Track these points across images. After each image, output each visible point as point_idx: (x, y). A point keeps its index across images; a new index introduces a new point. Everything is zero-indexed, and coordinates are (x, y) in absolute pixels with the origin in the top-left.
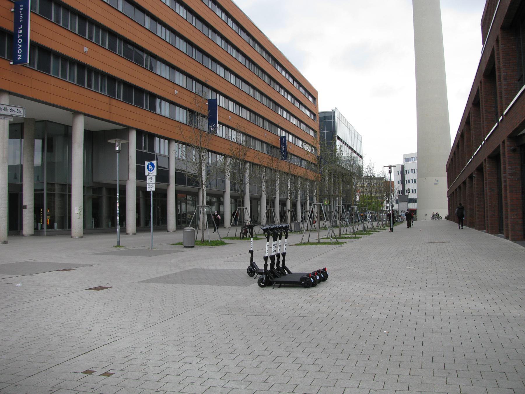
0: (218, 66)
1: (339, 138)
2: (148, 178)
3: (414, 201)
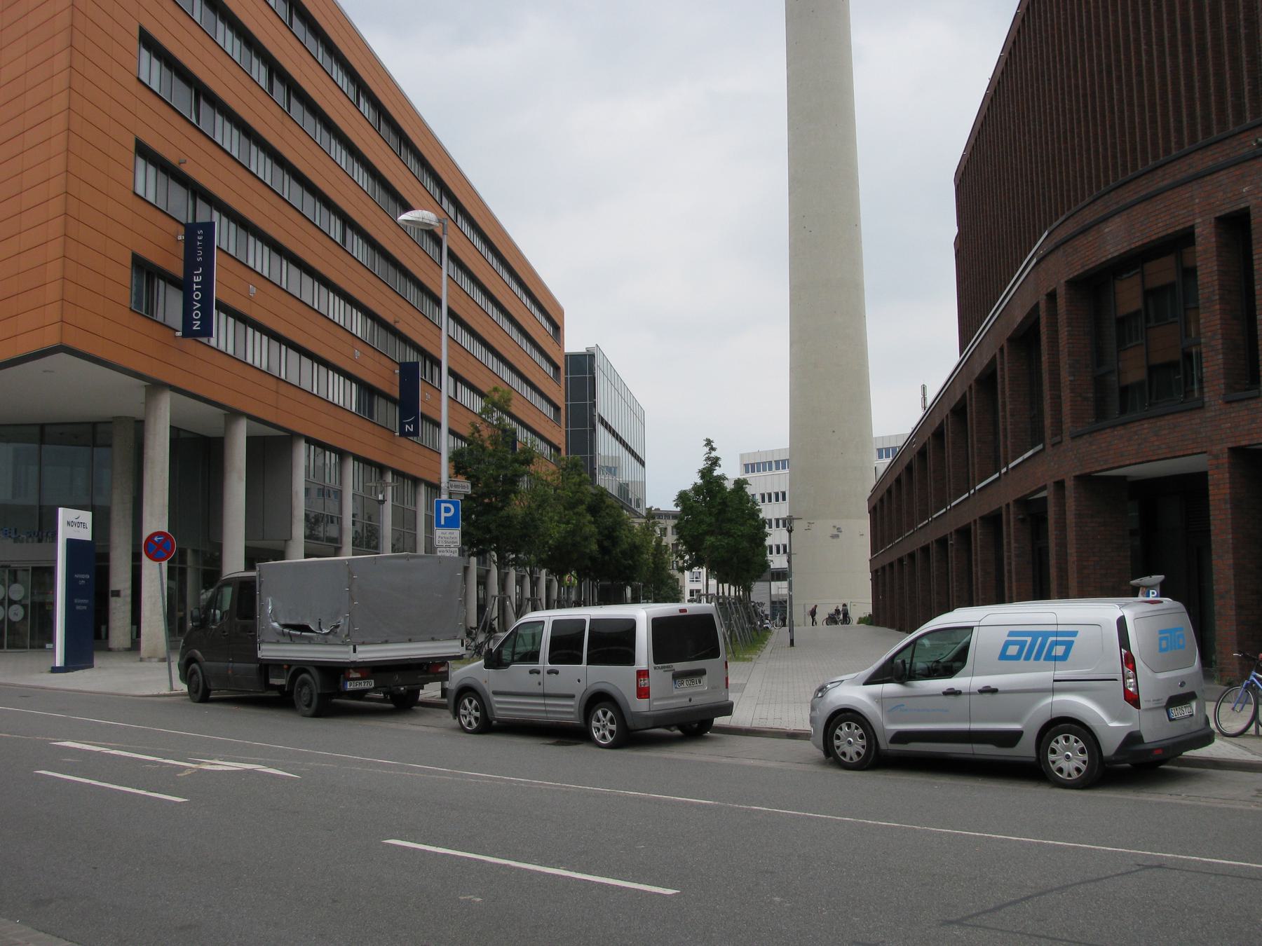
0: (219, 118)
1: (603, 421)
3: (781, 575)
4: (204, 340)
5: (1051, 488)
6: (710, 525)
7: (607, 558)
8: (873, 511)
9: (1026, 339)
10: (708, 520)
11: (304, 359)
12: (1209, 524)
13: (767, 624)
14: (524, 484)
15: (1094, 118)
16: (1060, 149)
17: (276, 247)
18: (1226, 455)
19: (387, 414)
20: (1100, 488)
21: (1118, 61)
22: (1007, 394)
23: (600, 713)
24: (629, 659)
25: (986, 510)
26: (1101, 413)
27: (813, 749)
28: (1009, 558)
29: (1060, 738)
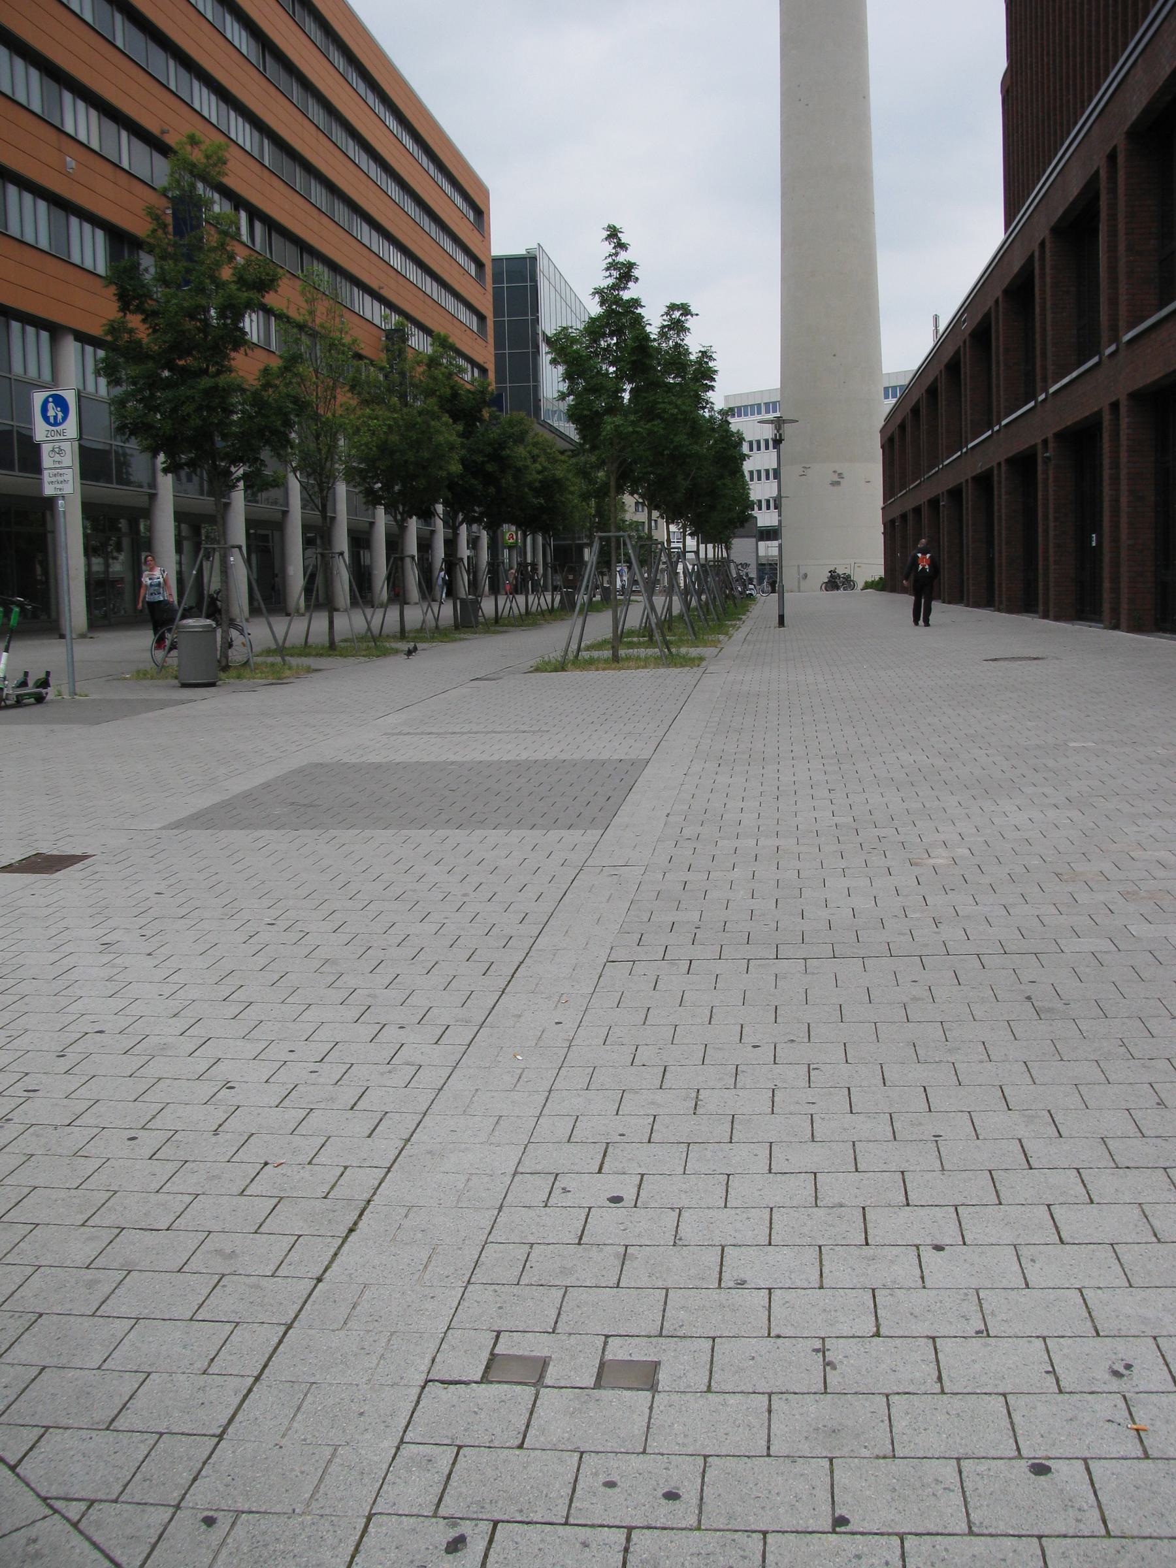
2: (46, 449)
3: (770, 534)
7: (492, 490)
13: (752, 589)
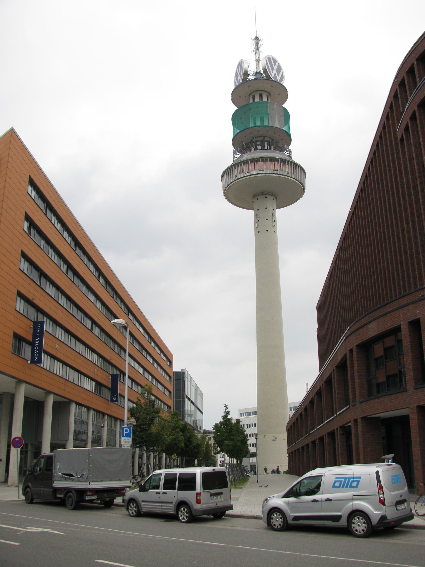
0: (48, 283)
1: (187, 397)
3: (254, 455)
4: (39, 364)
5: (353, 422)
6: (226, 437)
7: (188, 449)
8: (288, 431)
9: (342, 366)
10: (225, 435)
11: (76, 372)
12: (410, 435)
13: (249, 474)
14: (156, 421)
15: (365, 286)
16: (354, 297)
17: (67, 331)
18: (415, 409)
19: (106, 393)
20: (370, 421)
21: (373, 266)
22: (336, 387)
23: (182, 509)
24: (193, 487)
25: (329, 431)
26: (370, 394)
27: (263, 523)
28: (338, 448)
29: (356, 518)
